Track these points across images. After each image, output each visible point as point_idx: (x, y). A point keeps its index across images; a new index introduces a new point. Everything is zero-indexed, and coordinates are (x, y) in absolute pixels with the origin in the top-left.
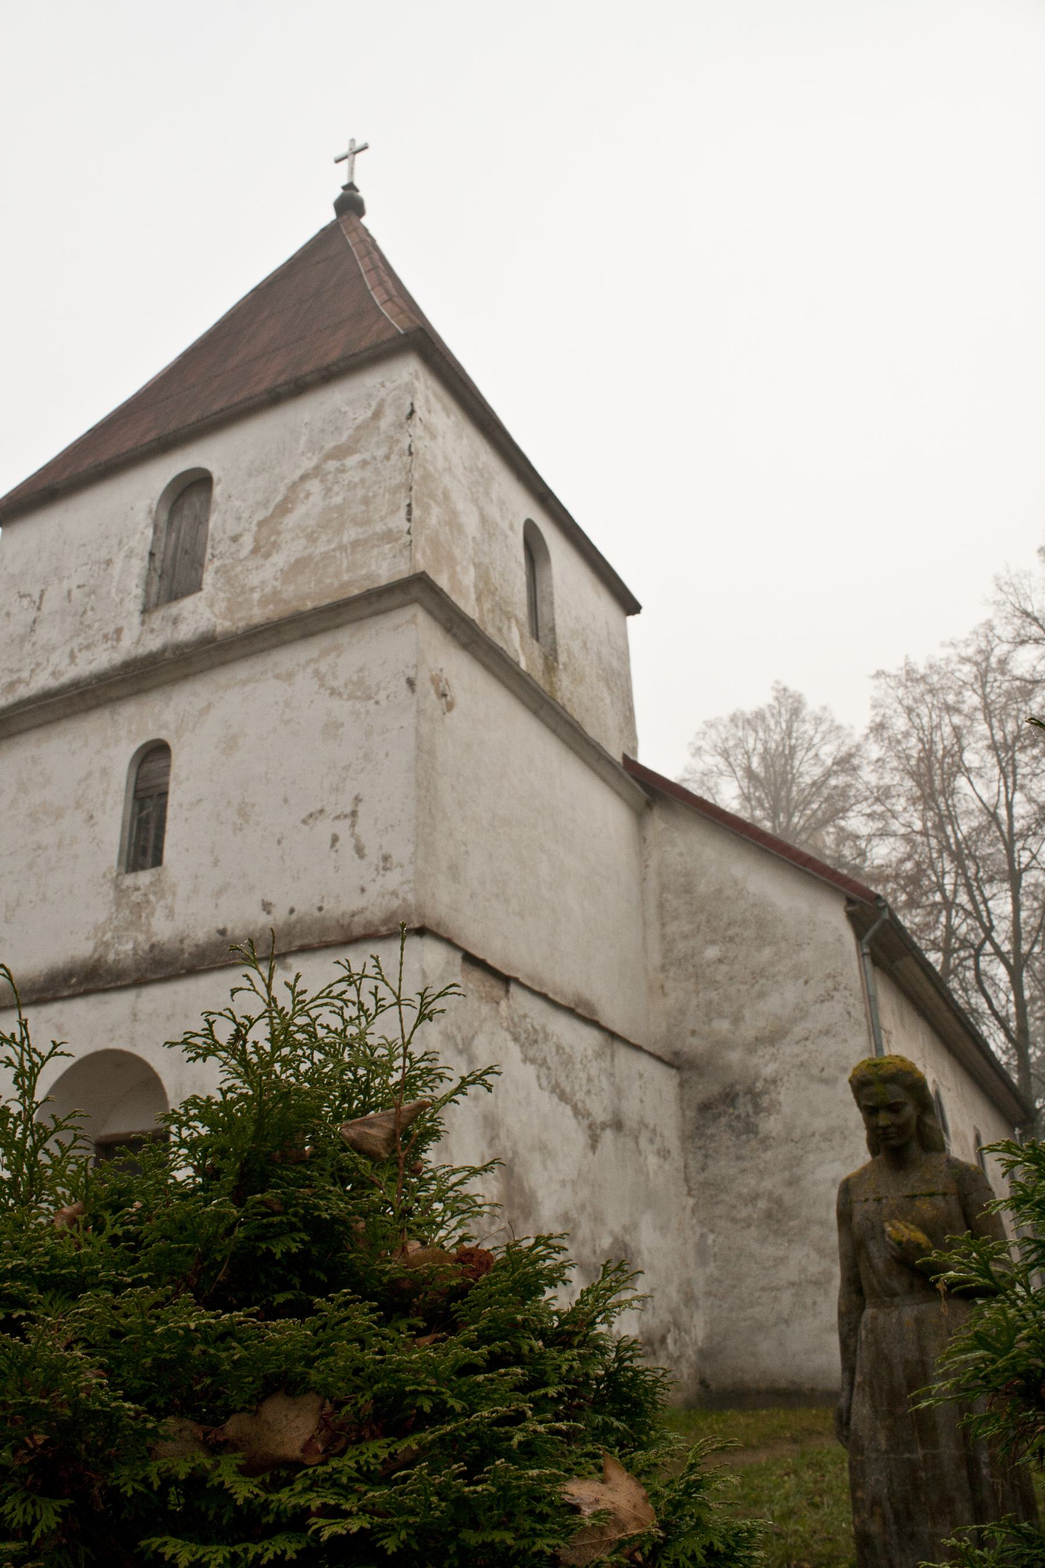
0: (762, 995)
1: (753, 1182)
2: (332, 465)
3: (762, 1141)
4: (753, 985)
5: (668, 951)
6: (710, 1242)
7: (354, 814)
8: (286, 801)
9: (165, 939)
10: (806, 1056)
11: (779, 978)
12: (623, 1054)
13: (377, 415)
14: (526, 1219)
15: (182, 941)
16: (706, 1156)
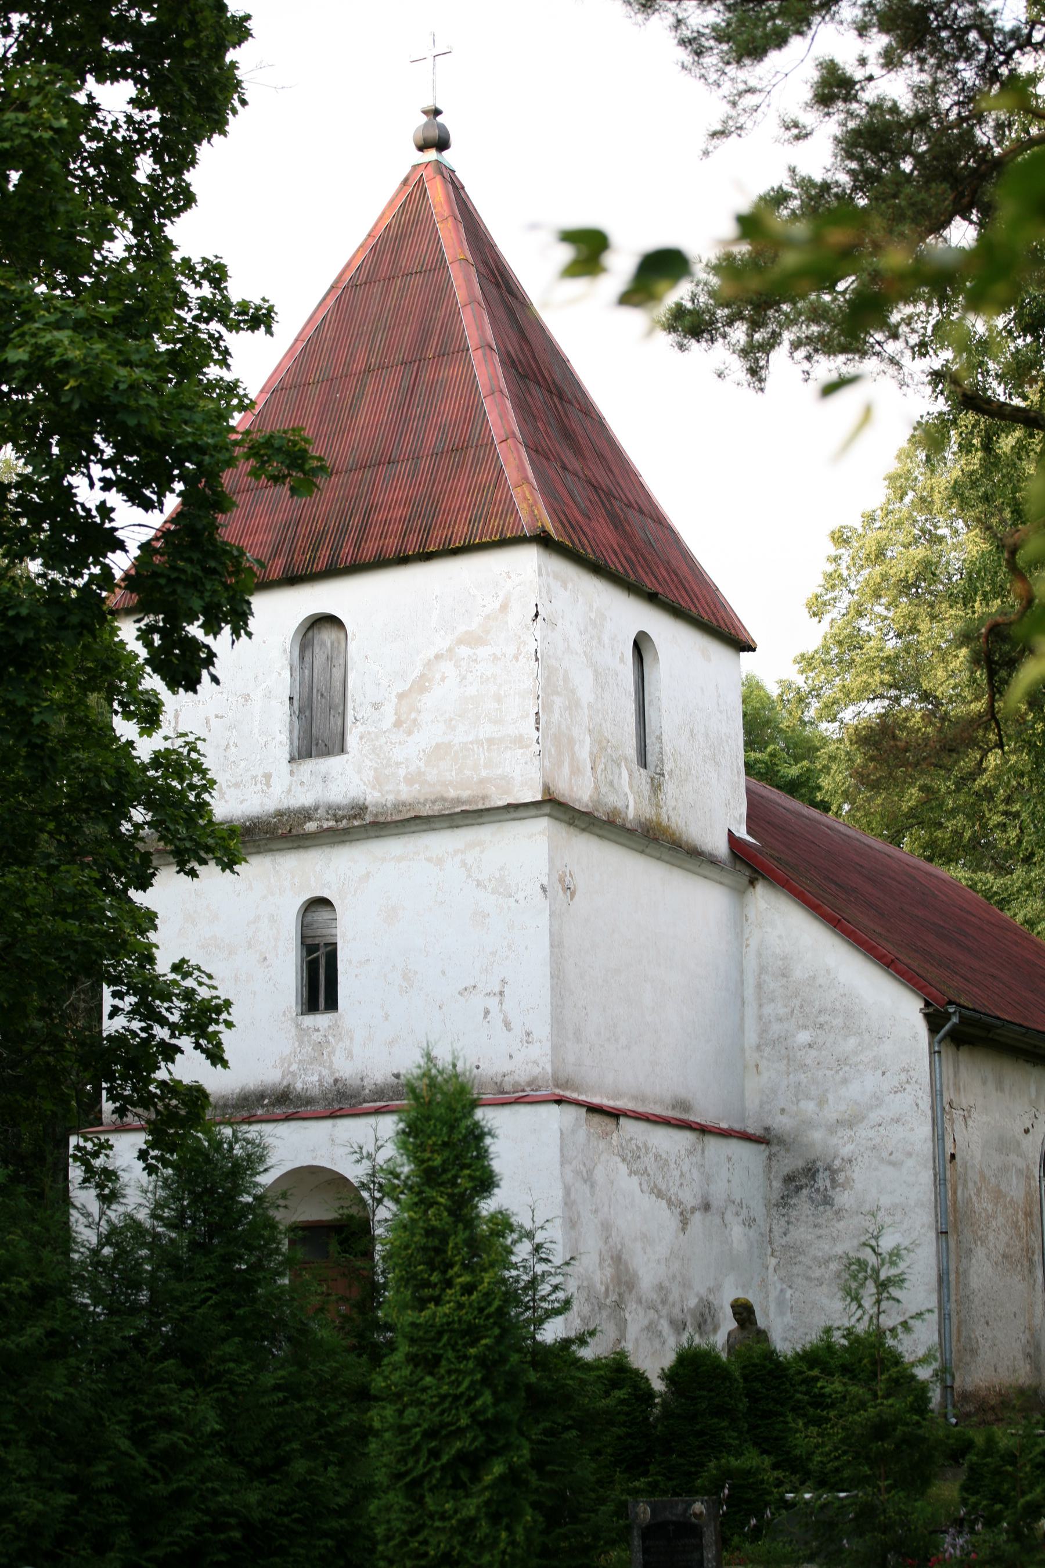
0: (845, 1081)
1: (827, 1247)
2: (464, 651)
3: (837, 1213)
4: (837, 1072)
5: (763, 1031)
6: (788, 1296)
7: (501, 993)
8: (444, 973)
9: (347, 1076)
10: (878, 1140)
11: (861, 1067)
12: (713, 1144)
13: (504, 608)
14: (630, 1292)
15: (362, 1079)
16: (788, 1223)
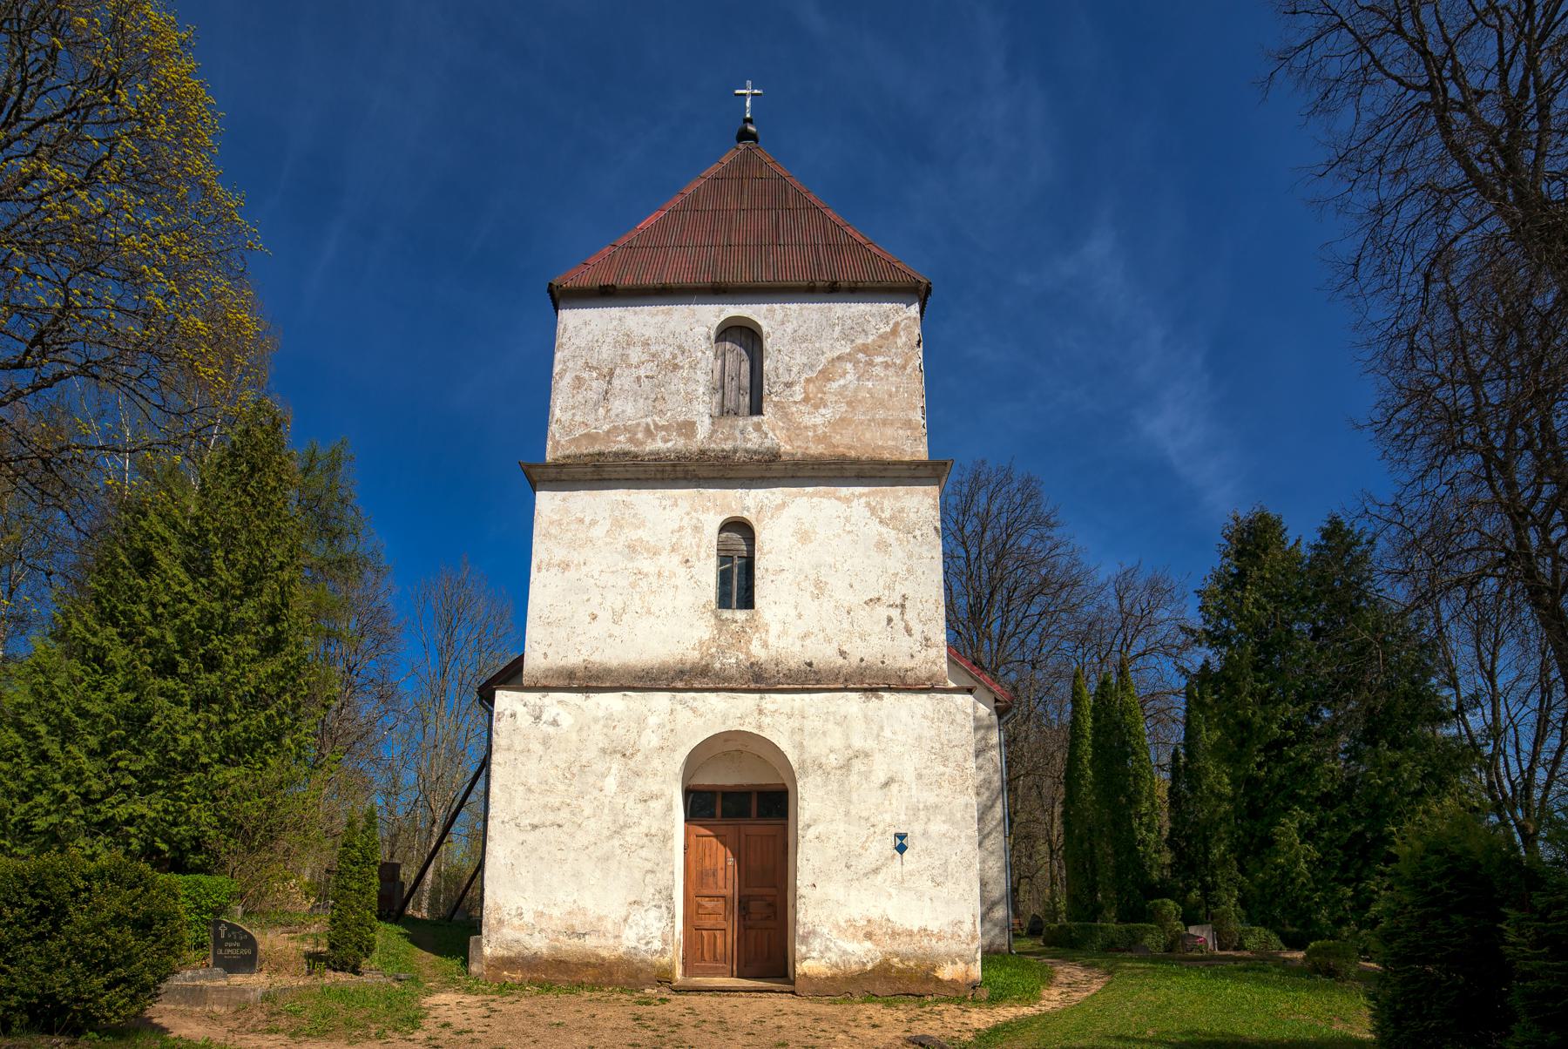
7: (903, 606)
13: (894, 332)
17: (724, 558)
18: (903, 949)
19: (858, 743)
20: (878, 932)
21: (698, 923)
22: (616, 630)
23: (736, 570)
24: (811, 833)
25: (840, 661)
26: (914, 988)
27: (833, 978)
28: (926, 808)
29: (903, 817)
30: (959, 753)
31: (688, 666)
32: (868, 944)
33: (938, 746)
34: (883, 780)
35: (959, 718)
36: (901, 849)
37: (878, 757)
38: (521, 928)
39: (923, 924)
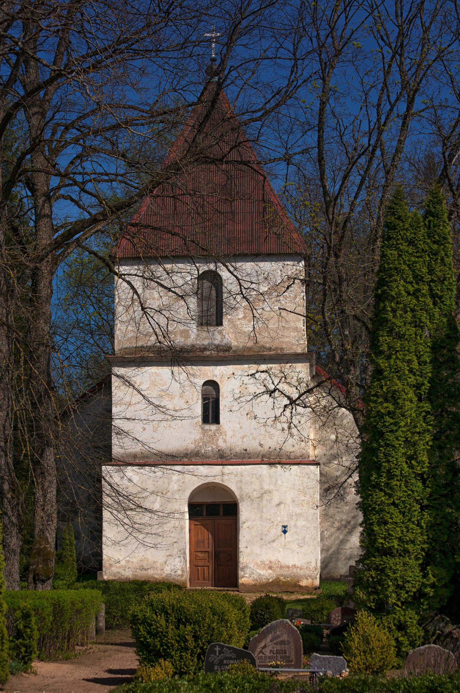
17: (205, 398)
18: (285, 573)
19: (266, 487)
20: (274, 566)
21: (196, 563)
22: (155, 435)
23: (211, 405)
24: (245, 526)
25: (260, 448)
26: (290, 589)
27: (255, 585)
28: (296, 515)
29: (285, 519)
30: (311, 491)
31: (189, 452)
32: (270, 571)
33: (302, 488)
34: (277, 503)
35: (312, 476)
36: (285, 532)
37: (275, 493)
38: (120, 567)
39: (294, 563)
